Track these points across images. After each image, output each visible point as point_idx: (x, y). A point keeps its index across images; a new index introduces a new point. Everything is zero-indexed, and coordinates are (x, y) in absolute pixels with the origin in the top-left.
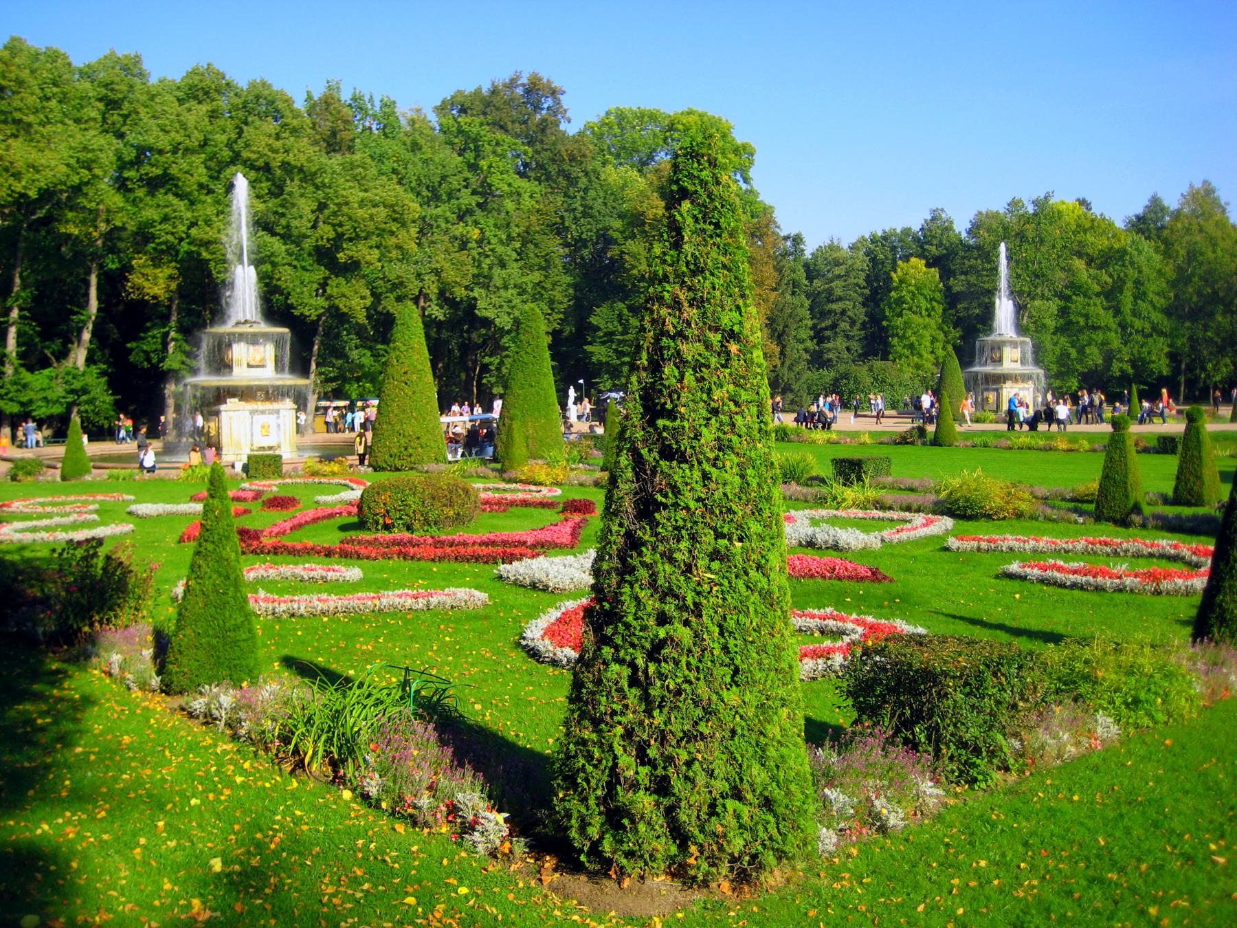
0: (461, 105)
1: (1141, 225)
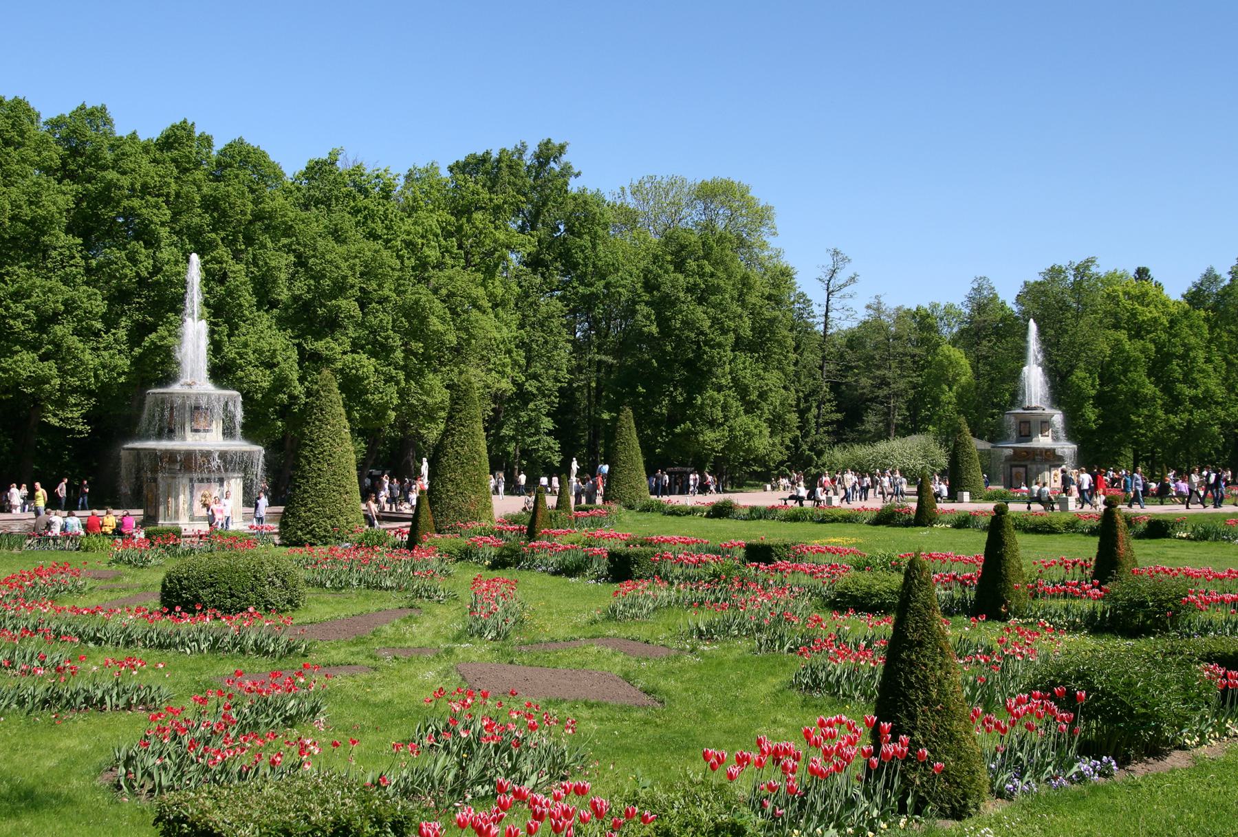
0: (473, 166)
1: (1195, 298)
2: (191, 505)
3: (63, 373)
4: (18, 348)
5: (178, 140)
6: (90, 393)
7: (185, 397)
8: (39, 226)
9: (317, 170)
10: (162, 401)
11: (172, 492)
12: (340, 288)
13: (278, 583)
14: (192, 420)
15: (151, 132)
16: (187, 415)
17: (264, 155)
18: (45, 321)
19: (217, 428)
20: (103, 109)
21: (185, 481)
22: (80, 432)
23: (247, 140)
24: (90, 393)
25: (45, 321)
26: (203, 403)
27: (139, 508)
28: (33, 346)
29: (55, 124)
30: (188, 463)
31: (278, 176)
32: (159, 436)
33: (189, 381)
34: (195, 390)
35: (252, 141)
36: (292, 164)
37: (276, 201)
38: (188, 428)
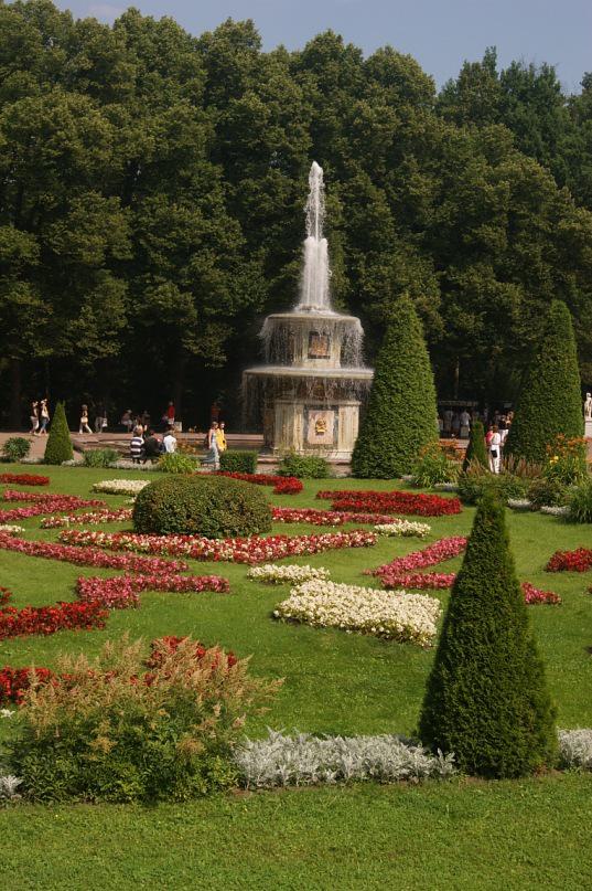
2: (306, 433)
3: (199, 304)
4: (158, 278)
5: (322, 59)
6: (229, 320)
7: (301, 321)
8: (183, 157)
9: (473, 76)
10: (282, 326)
11: (286, 416)
12: (486, 214)
13: (235, 507)
14: (310, 346)
15: (297, 44)
16: (305, 341)
17: (414, 69)
18: (183, 253)
19: (335, 354)
20: (249, 25)
21: (301, 407)
22: (217, 362)
23: (395, 49)
24: (229, 320)
25: (183, 253)
26: (319, 329)
27: (261, 433)
28: (173, 275)
29: (202, 45)
30: (300, 387)
31: (427, 85)
32: (273, 361)
33: (307, 305)
34: (313, 314)
35: (401, 48)
36: (442, 72)
37: (425, 121)
38: (305, 356)
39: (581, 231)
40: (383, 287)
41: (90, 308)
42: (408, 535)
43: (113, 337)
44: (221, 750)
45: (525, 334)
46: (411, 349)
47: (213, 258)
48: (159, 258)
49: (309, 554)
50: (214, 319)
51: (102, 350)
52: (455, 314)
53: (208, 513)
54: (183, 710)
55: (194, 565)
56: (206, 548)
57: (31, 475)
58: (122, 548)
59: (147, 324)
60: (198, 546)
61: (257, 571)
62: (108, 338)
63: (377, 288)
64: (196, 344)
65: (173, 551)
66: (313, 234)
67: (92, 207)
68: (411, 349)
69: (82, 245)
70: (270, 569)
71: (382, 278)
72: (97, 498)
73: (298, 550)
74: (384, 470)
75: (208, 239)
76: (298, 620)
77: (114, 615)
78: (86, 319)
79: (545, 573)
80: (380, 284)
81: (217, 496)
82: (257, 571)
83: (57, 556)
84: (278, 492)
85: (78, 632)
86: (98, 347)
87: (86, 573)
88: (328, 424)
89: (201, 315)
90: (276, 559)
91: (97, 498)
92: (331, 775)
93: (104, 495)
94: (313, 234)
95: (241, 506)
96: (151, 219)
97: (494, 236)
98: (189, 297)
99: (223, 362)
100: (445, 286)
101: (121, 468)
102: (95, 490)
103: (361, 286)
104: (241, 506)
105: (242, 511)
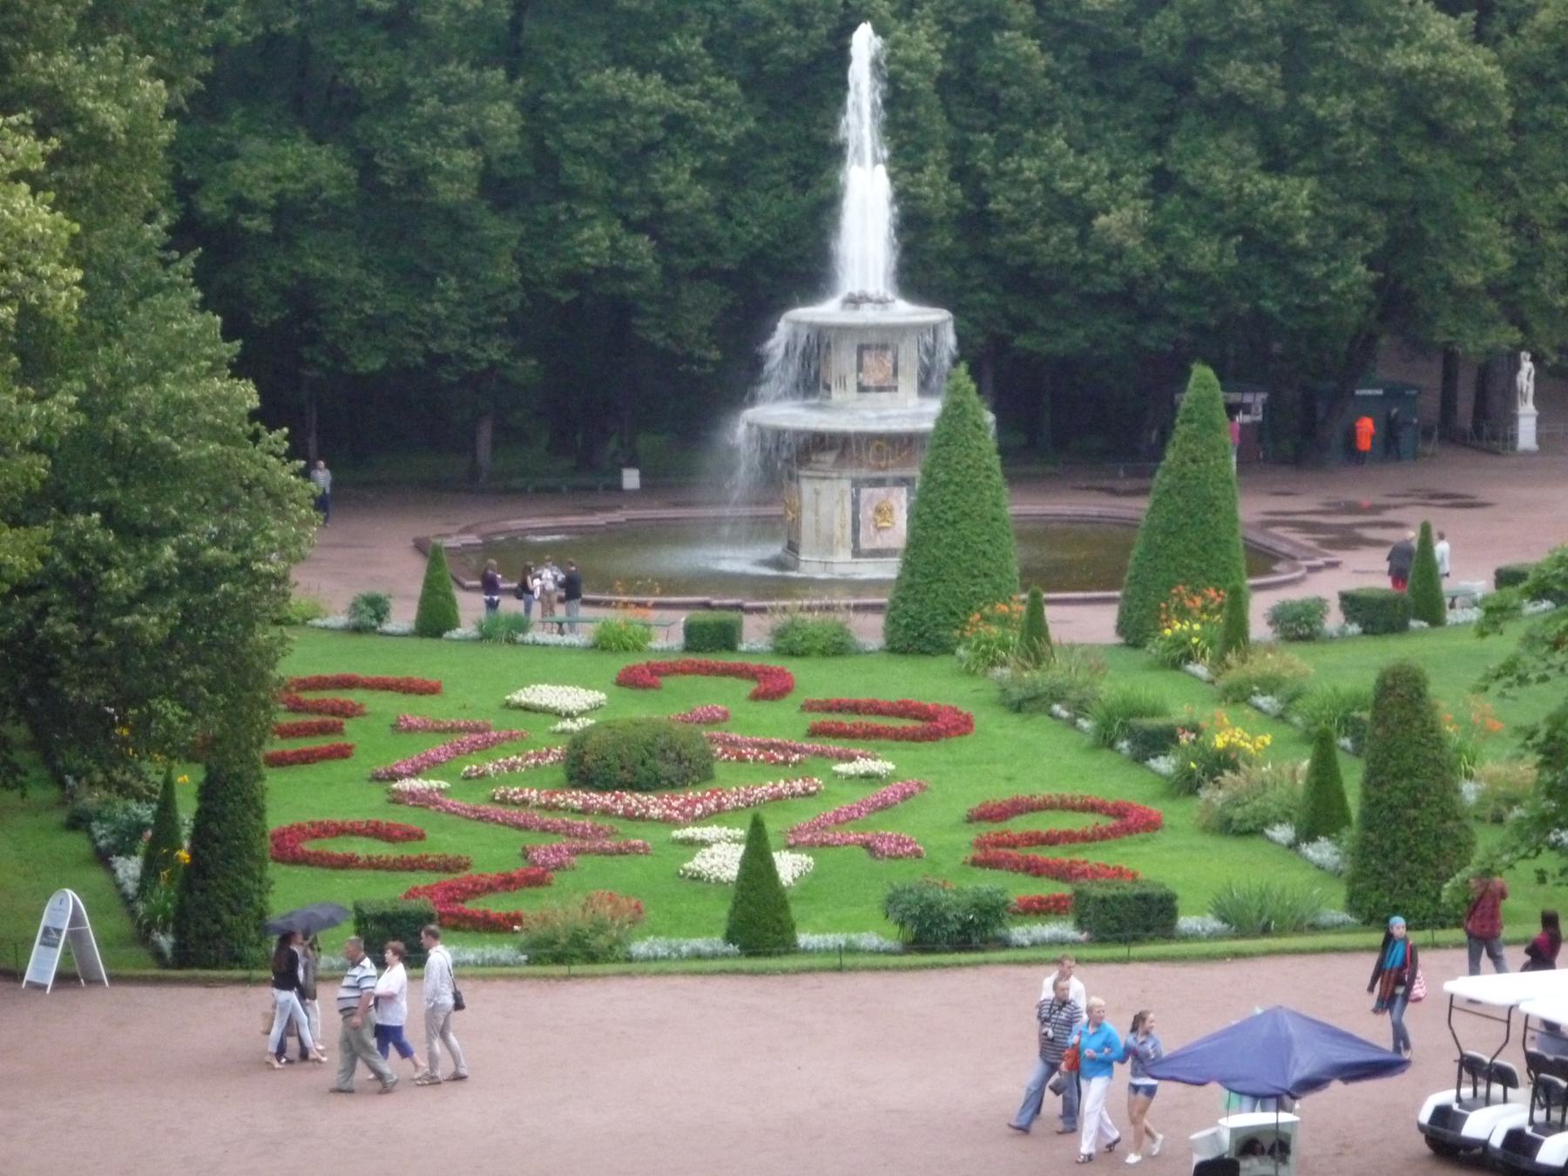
3: (664, 247)
6: (725, 277)
13: (673, 755)
18: (636, 158)
24: (725, 277)
25: (636, 158)
39: (1432, 69)
40: (1027, 201)
41: (453, 280)
42: (868, 777)
43: (498, 329)
44: (618, 942)
45: (1327, 275)
46: (967, 455)
47: (691, 162)
48: (582, 173)
49: (741, 808)
50: (698, 274)
51: (479, 355)
52: (1183, 243)
53: (643, 763)
54: (600, 928)
55: (622, 826)
56: (637, 808)
57: (415, 677)
58: (555, 807)
59: (566, 297)
60: (630, 805)
61: (678, 834)
62: (487, 330)
63: (1017, 204)
64: (661, 328)
65: (606, 812)
66: (861, 163)
67: (451, 93)
68: (967, 455)
69: (437, 169)
70: (690, 832)
71: (1027, 185)
72: (516, 721)
73: (728, 806)
74: (929, 641)
75: (676, 124)
76: (697, 878)
77: (556, 877)
78: (445, 301)
79: (967, 826)
80: (1024, 195)
81: (652, 745)
82: (678, 834)
83: (495, 820)
84: (756, 697)
85: (533, 890)
86: (470, 351)
87: (529, 839)
88: (896, 513)
89: (669, 272)
90: (697, 820)
91: (516, 721)
92: (675, 955)
93: (520, 713)
94: (861, 163)
95: (679, 755)
96: (565, 95)
97: (1257, 85)
98: (643, 244)
99: (714, 363)
100: (1162, 181)
101: (535, 644)
102: (508, 706)
103: (985, 198)
104: (679, 755)
105: (680, 759)
